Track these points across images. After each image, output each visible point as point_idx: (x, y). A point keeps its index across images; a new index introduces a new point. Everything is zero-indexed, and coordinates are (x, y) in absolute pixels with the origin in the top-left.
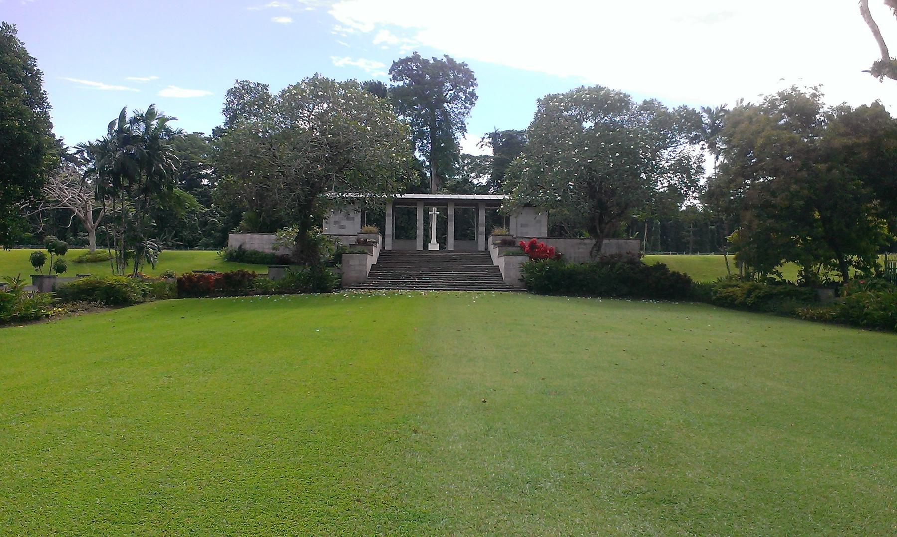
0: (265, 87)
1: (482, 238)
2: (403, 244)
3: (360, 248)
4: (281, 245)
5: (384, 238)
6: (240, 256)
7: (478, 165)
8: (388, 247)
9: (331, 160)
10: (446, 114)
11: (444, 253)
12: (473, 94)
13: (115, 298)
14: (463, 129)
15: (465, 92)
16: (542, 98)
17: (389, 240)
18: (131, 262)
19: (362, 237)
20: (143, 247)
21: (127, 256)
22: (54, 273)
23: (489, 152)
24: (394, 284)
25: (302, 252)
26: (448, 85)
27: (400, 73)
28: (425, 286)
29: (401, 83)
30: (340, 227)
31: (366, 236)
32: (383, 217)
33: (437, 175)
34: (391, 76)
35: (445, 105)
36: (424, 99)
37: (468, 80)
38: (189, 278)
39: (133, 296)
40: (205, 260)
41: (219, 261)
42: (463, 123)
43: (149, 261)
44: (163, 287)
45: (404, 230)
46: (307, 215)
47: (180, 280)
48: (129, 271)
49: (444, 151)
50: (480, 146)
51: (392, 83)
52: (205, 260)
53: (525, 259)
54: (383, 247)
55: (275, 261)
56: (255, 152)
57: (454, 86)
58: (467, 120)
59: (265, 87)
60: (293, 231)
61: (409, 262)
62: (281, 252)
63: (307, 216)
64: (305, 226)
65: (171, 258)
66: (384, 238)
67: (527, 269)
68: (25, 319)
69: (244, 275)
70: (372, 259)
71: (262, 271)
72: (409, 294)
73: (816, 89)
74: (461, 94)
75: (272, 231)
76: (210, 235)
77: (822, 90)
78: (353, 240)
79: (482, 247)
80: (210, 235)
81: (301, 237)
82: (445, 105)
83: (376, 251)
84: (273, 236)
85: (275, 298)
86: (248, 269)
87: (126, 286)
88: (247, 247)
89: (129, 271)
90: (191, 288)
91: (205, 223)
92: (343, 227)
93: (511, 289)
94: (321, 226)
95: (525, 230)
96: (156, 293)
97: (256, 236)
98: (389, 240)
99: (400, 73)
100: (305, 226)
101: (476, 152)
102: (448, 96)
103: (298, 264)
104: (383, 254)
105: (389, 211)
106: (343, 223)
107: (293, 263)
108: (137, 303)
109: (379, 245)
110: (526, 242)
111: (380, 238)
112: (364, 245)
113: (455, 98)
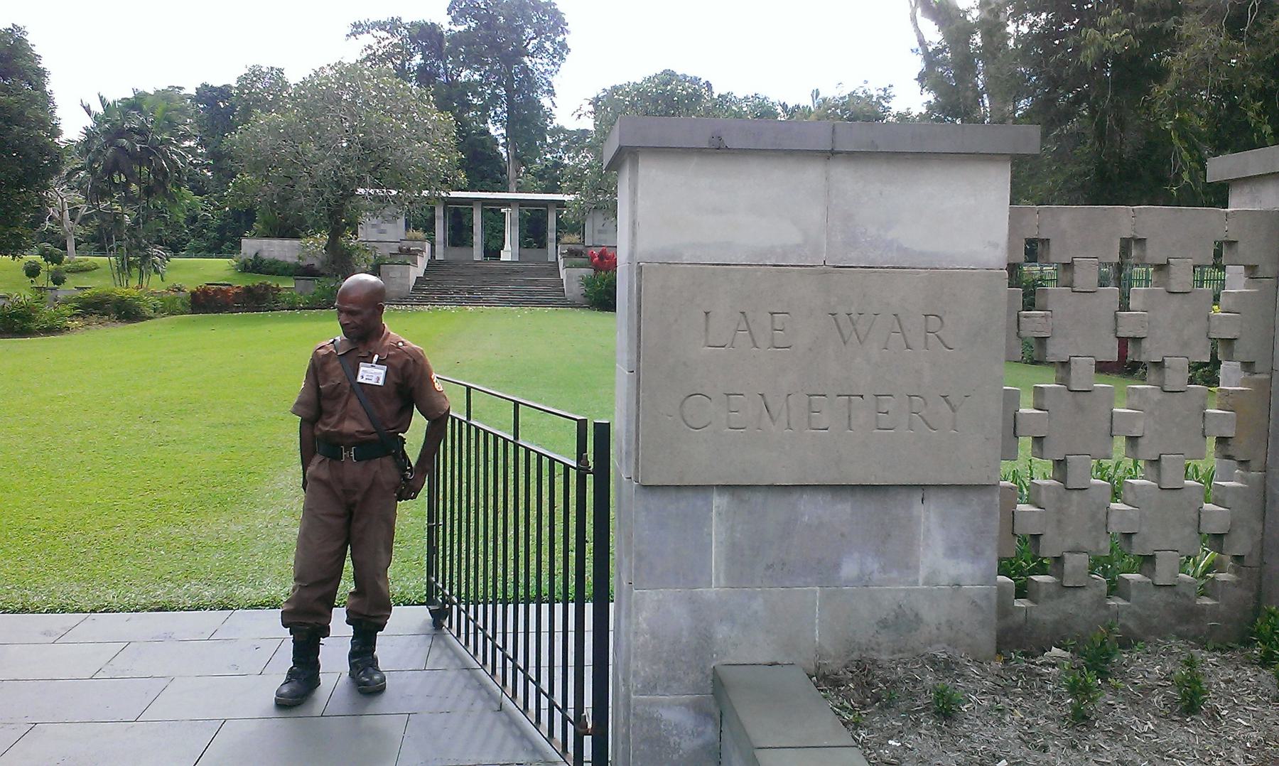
0: (280, 71)
1: (551, 246)
2: (457, 253)
3: (401, 258)
4: (308, 253)
5: (433, 245)
6: (256, 266)
7: (577, 140)
8: (439, 256)
9: (362, 161)
10: (526, 70)
11: (494, 264)
12: (563, 46)
13: (127, 312)
14: (551, 93)
15: (553, 42)
16: (608, 88)
17: (439, 249)
18: (135, 270)
19: (405, 245)
20: (148, 256)
21: (130, 264)
22: (51, 285)
23: (588, 124)
24: (440, 298)
25: (334, 262)
26: (530, 32)
27: (463, 13)
28: (475, 301)
29: (462, 28)
30: (379, 232)
31: (410, 243)
32: (432, 221)
33: (516, 157)
34: (449, 18)
35: (526, 59)
36: (495, 47)
37: (557, 25)
38: (205, 292)
39: (148, 312)
40: (215, 270)
41: (228, 273)
42: (550, 84)
43: (157, 271)
44: (173, 301)
45: (459, 235)
46: (339, 218)
47: (193, 294)
48: (134, 283)
49: (527, 121)
50: (576, 115)
51: (453, 27)
52: (215, 270)
53: (587, 272)
54: (433, 256)
55: (304, 272)
56: (275, 150)
57: (538, 33)
58: (555, 80)
59: (280, 71)
60: (323, 238)
61: (461, 275)
62: (309, 261)
63: (337, 222)
64: (335, 234)
65: (175, 268)
66: (433, 245)
67: (588, 283)
68: (50, 331)
69: (267, 287)
70: (418, 269)
71: (287, 284)
72: (454, 309)
73: (885, 90)
74: (547, 45)
75: (296, 236)
76: (201, 235)
77: (892, 91)
78: (394, 248)
79: (551, 259)
80: (201, 235)
81: (332, 246)
82: (526, 59)
83: (422, 262)
84: (296, 242)
85: (306, 313)
86: (271, 281)
87: (138, 299)
88: (265, 255)
89: (134, 283)
90: (206, 302)
91: (193, 219)
92: (383, 232)
93: (573, 305)
94: (355, 233)
95: (603, 236)
96: (167, 309)
97: (276, 242)
98: (439, 249)
99: (463, 13)
100: (335, 234)
101: (572, 125)
102: (529, 47)
103: (330, 276)
104: (432, 265)
105: (439, 212)
106: (383, 227)
107: (323, 274)
108: (150, 318)
109: (427, 255)
110: (596, 252)
111: (428, 246)
112: (407, 255)
113: (540, 48)
